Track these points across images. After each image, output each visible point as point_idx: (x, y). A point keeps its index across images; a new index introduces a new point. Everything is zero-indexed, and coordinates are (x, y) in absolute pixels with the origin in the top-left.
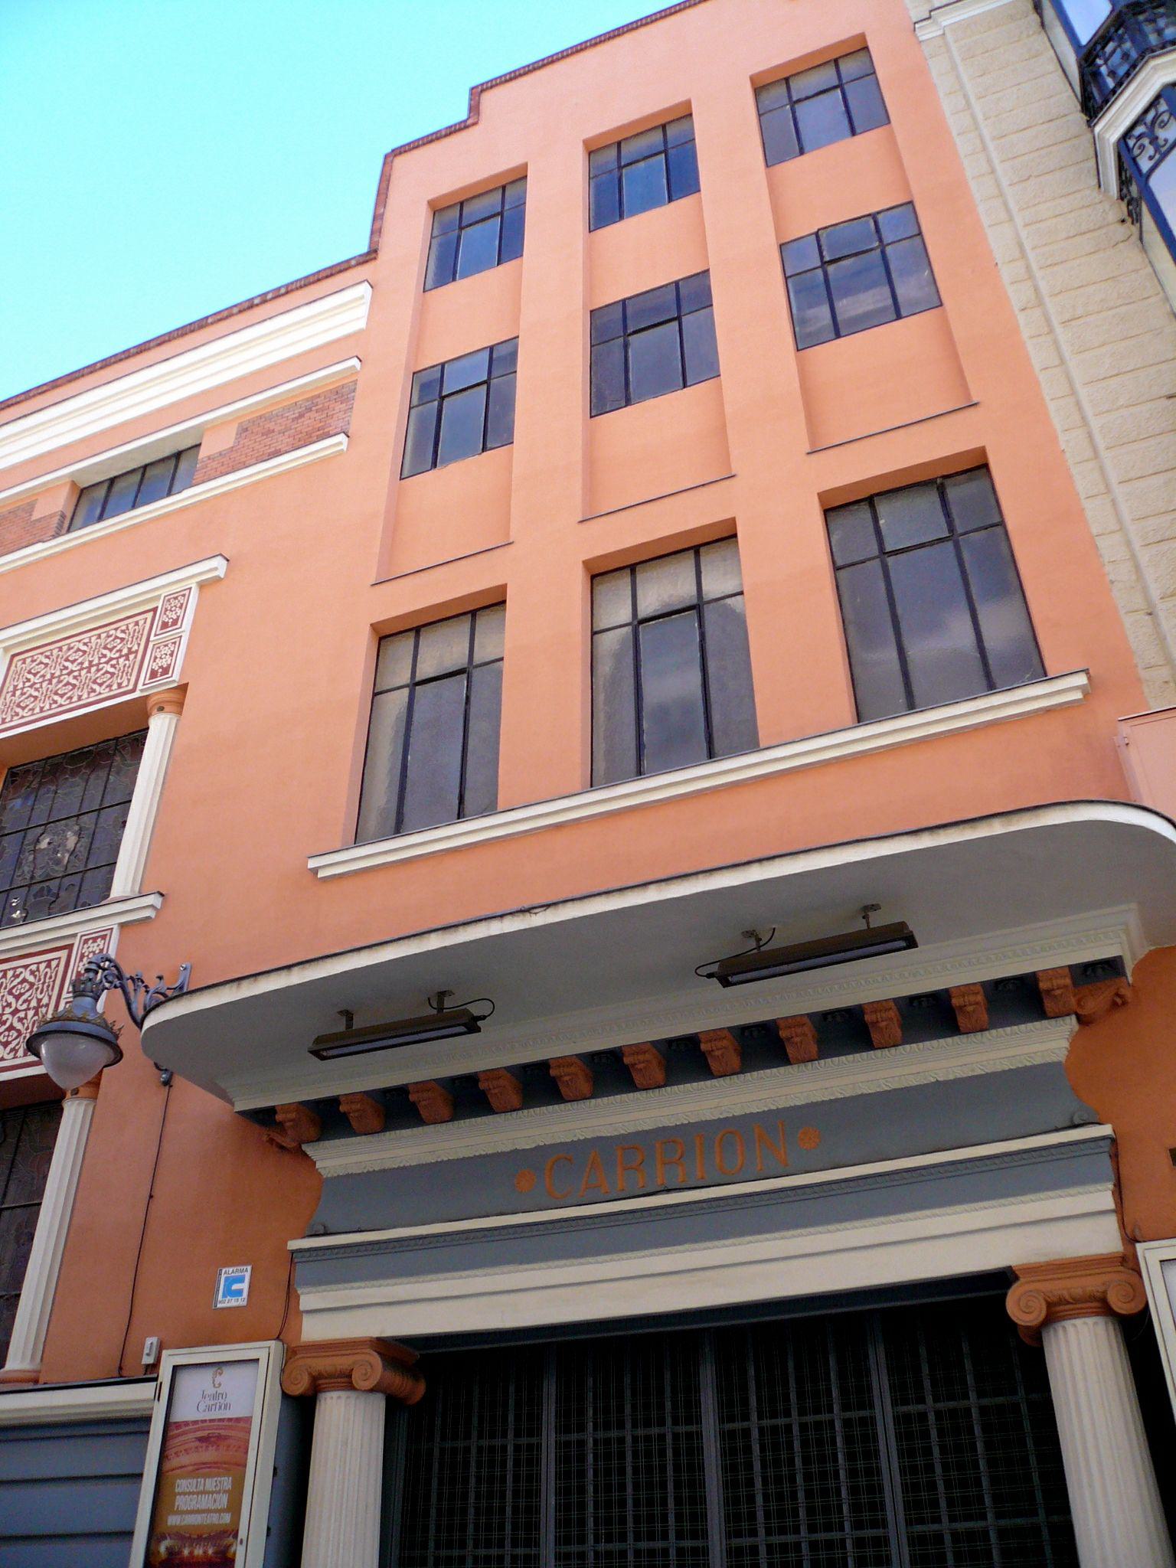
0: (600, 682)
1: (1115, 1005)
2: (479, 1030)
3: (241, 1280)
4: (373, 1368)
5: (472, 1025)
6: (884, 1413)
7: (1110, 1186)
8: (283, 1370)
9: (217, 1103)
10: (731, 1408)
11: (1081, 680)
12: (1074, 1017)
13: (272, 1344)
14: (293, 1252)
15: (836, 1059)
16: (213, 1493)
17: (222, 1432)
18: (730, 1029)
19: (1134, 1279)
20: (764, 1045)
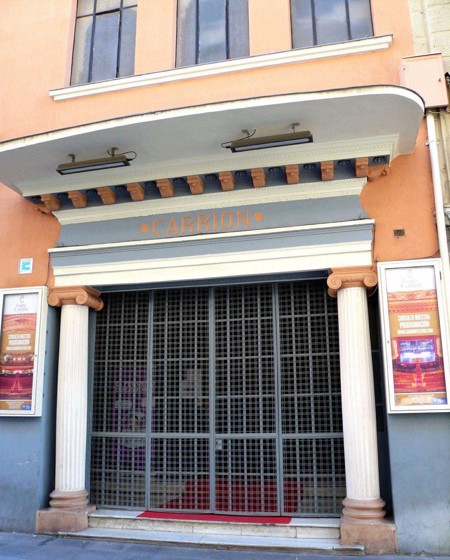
0: (180, 23)
1: (382, 175)
2: (129, 165)
3: (29, 263)
4: (85, 297)
5: (126, 162)
6: (276, 317)
7: (371, 241)
8: (48, 297)
9: (15, 194)
10: (220, 314)
11: (389, 39)
12: (366, 178)
13: (44, 287)
14: (50, 253)
15: (272, 187)
16: (23, 339)
17: (25, 318)
18: (231, 172)
19: (375, 274)
20: (244, 179)
